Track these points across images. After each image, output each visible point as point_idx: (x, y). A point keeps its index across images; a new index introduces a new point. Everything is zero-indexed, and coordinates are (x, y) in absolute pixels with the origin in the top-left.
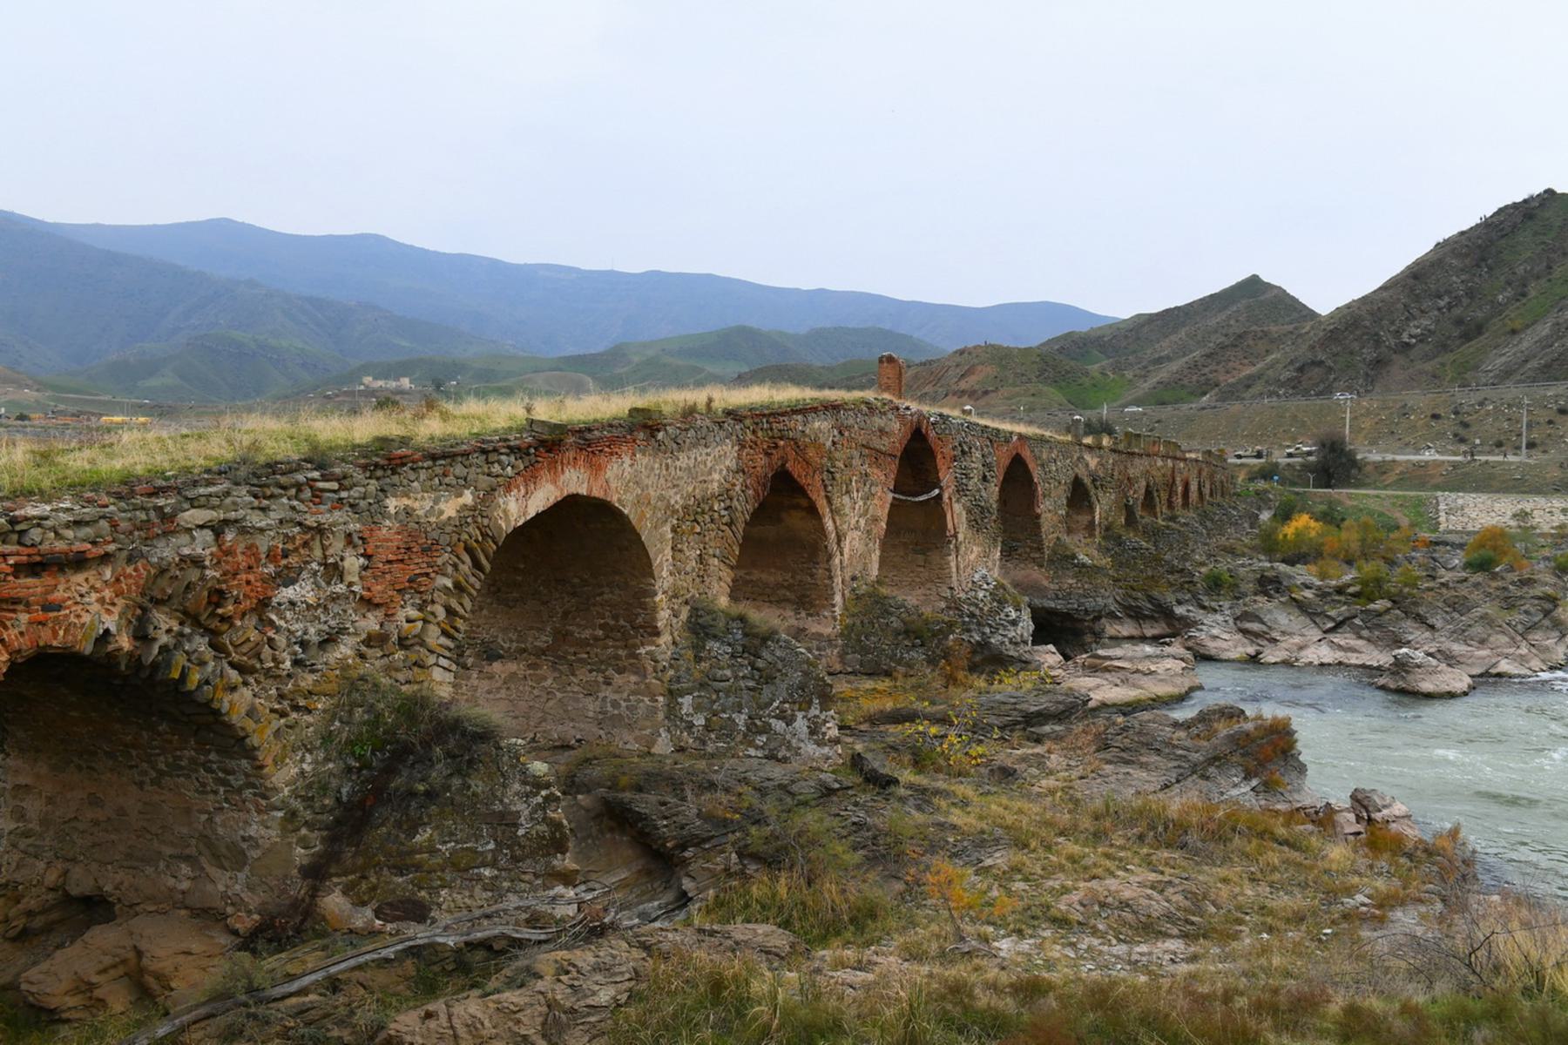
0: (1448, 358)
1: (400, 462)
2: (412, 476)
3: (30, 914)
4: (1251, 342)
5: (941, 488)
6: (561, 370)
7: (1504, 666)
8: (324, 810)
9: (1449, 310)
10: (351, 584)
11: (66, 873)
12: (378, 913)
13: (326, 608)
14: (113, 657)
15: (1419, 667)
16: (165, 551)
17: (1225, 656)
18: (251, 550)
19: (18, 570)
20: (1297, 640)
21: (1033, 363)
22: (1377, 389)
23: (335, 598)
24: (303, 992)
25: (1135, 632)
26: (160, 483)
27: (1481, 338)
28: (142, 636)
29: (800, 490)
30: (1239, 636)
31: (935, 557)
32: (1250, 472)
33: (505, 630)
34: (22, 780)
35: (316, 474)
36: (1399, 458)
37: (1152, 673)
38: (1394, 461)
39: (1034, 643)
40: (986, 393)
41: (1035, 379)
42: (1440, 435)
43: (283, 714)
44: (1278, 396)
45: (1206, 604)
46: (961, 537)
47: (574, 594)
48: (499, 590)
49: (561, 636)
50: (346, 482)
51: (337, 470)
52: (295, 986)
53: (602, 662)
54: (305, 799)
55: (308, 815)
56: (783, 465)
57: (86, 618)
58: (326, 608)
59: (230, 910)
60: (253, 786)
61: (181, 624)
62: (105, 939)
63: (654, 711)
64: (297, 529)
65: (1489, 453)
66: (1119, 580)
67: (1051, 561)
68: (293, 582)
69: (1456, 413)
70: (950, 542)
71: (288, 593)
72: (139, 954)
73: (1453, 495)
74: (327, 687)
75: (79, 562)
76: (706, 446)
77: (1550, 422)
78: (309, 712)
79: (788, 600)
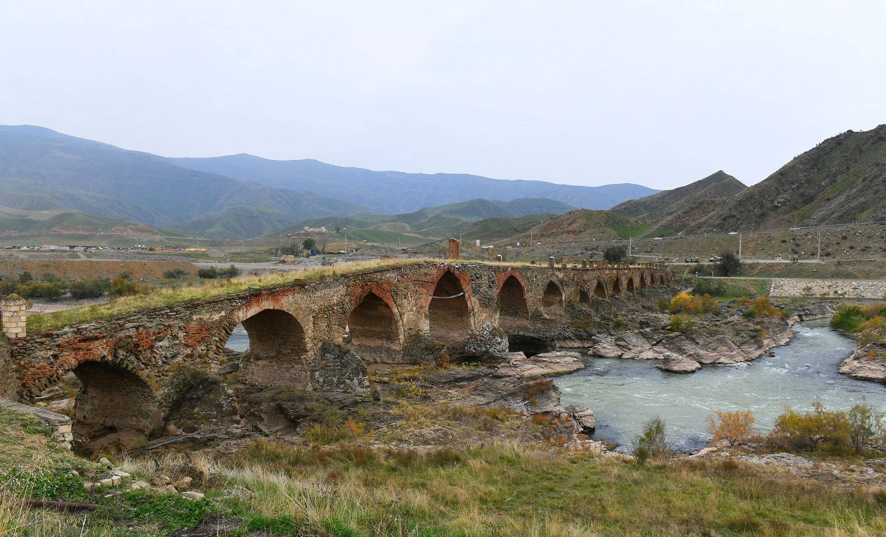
0: (796, 213)
1: (198, 305)
2: (202, 309)
3: (96, 431)
4: (706, 206)
5: (464, 292)
6: (396, 221)
7: (723, 360)
8: (169, 403)
9: (798, 189)
10: (180, 341)
11: (105, 420)
12: (184, 431)
13: (172, 347)
14: (107, 362)
15: (673, 360)
16: (121, 334)
17: (608, 355)
18: (148, 333)
19: (80, 341)
20: (639, 349)
21: (603, 217)
22: (761, 228)
23: (176, 345)
24: (157, 448)
25: (580, 345)
26: (121, 317)
27: (813, 203)
28: (115, 356)
29: (380, 299)
30: (616, 347)
31: (465, 318)
32: (690, 269)
33: (262, 350)
34: (93, 395)
35: (169, 311)
36: (761, 261)
37: (558, 363)
38: (758, 263)
39: (510, 351)
40: (581, 232)
41: (603, 225)
42: (786, 250)
43: (159, 377)
44: (713, 232)
45: (612, 333)
46: (476, 310)
47: (281, 339)
48: (260, 337)
49: (279, 352)
50: (178, 312)
51: (175, 309)
52: (154, 447)
53: (290, 361)
54: (165, 400)
55: (165, 404)
56: (371, 291)
57: (99, 352)
58: (172, 347)
59: (146, 430)
60: (150, 396)
61: (127, 353)
62: (112, 437)
63: (306, 377)
64: (162, 326)
65: (807, 258)
66: (573, 324)
67: (532, 317)
68: (162, 341)
69: (794, 240)
70: (470, 313)
71: (161, 344)
72: (120, 440)
73: (779, 279)
74: (173, 370)
75: (97, 338)
76: (330, 288)
77: (838, 243)
78: (167, 376)
79: (384, 337)
